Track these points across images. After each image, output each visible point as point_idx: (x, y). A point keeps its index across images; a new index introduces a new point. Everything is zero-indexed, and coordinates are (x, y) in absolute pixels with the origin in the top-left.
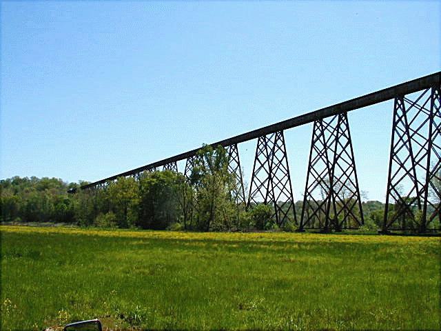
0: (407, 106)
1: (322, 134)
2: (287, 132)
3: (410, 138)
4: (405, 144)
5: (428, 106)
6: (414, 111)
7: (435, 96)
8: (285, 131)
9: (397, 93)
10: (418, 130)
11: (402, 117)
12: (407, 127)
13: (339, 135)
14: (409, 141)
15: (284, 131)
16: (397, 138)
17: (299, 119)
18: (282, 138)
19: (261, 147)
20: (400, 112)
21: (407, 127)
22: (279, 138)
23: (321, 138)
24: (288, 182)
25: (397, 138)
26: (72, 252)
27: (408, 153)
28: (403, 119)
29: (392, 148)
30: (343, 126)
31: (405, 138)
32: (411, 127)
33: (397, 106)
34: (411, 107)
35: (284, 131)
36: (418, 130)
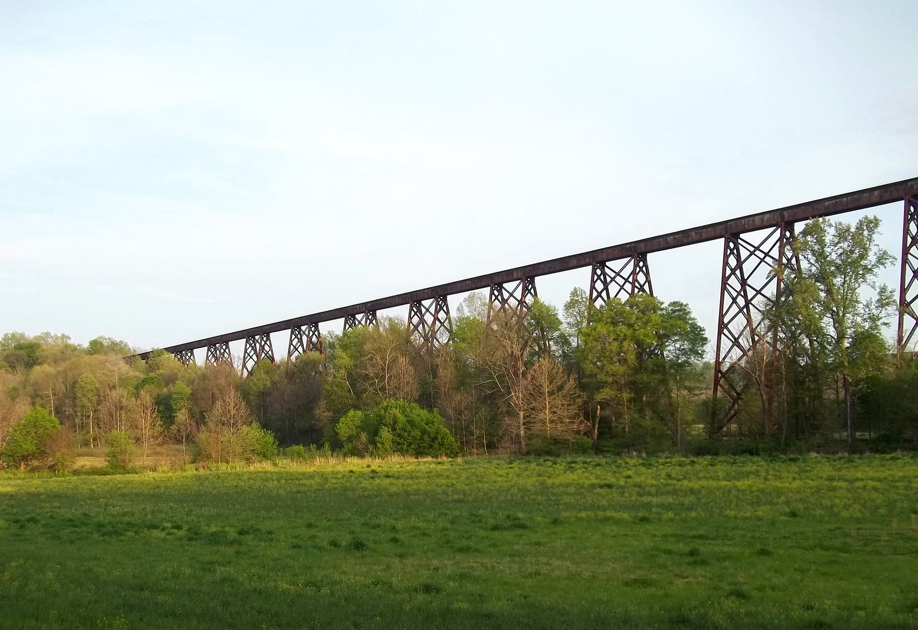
0: (744, 254)
1: (606, 288)
2: (541, 281)
3: (748, 302)
4: (741, 310)
5: (775, 253)
6: (754, 261)
7: (729, 251)
8: (271, 334)
9: (730, 231)
10: (762, 289)
11: (602, 291)
12: (744, 282)
13: (636, 290)
14: (747, 306)
15: (378, 312)
16: (728, 300)
17: (478, 285)
18: (445, 308)
19: (294, 343)
20: (732, 261)
21: (744, 282)
22: (441, 308)
23: (420, 328)
24: (722, 356)
25: (728, 300)
26: (753, 572)
27: (745, 322)
28: (604, 294)
29: (722, 316)
30: (641, 278)
31: (741, 301)
32: (749, 282)
33: (596, 277)
34: (750, 255)
35: (378, 312)
36: (762, 289)
